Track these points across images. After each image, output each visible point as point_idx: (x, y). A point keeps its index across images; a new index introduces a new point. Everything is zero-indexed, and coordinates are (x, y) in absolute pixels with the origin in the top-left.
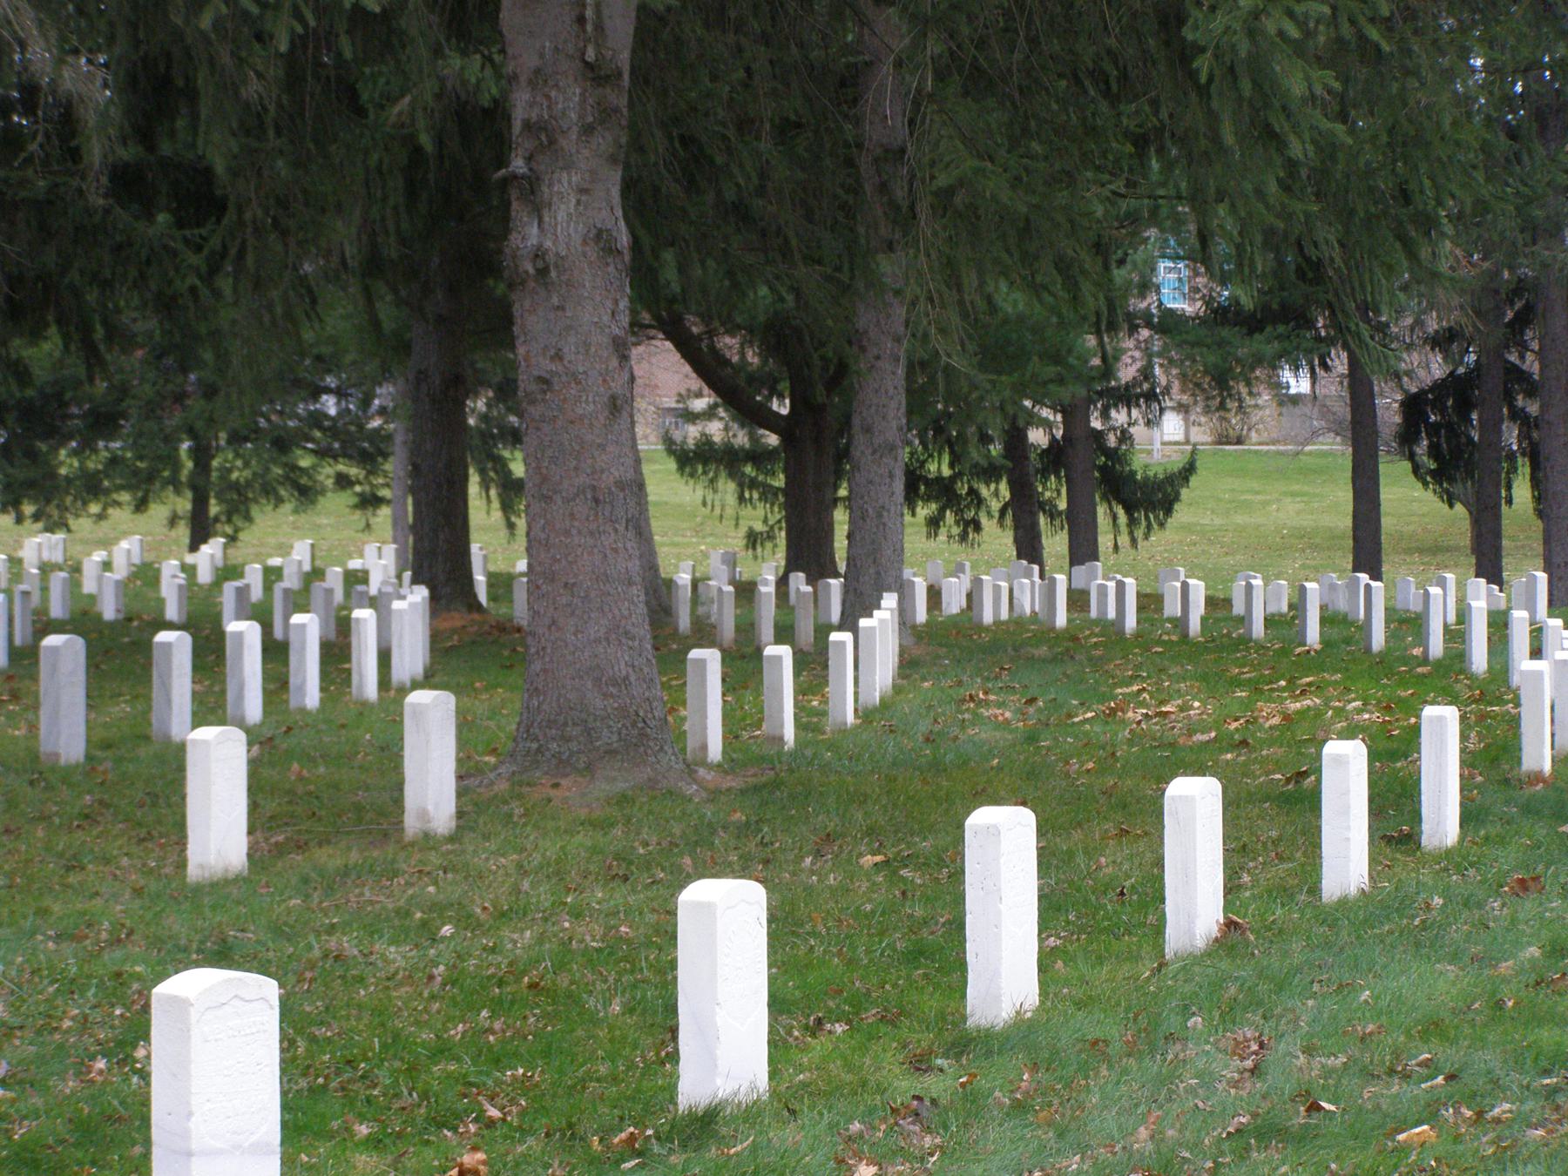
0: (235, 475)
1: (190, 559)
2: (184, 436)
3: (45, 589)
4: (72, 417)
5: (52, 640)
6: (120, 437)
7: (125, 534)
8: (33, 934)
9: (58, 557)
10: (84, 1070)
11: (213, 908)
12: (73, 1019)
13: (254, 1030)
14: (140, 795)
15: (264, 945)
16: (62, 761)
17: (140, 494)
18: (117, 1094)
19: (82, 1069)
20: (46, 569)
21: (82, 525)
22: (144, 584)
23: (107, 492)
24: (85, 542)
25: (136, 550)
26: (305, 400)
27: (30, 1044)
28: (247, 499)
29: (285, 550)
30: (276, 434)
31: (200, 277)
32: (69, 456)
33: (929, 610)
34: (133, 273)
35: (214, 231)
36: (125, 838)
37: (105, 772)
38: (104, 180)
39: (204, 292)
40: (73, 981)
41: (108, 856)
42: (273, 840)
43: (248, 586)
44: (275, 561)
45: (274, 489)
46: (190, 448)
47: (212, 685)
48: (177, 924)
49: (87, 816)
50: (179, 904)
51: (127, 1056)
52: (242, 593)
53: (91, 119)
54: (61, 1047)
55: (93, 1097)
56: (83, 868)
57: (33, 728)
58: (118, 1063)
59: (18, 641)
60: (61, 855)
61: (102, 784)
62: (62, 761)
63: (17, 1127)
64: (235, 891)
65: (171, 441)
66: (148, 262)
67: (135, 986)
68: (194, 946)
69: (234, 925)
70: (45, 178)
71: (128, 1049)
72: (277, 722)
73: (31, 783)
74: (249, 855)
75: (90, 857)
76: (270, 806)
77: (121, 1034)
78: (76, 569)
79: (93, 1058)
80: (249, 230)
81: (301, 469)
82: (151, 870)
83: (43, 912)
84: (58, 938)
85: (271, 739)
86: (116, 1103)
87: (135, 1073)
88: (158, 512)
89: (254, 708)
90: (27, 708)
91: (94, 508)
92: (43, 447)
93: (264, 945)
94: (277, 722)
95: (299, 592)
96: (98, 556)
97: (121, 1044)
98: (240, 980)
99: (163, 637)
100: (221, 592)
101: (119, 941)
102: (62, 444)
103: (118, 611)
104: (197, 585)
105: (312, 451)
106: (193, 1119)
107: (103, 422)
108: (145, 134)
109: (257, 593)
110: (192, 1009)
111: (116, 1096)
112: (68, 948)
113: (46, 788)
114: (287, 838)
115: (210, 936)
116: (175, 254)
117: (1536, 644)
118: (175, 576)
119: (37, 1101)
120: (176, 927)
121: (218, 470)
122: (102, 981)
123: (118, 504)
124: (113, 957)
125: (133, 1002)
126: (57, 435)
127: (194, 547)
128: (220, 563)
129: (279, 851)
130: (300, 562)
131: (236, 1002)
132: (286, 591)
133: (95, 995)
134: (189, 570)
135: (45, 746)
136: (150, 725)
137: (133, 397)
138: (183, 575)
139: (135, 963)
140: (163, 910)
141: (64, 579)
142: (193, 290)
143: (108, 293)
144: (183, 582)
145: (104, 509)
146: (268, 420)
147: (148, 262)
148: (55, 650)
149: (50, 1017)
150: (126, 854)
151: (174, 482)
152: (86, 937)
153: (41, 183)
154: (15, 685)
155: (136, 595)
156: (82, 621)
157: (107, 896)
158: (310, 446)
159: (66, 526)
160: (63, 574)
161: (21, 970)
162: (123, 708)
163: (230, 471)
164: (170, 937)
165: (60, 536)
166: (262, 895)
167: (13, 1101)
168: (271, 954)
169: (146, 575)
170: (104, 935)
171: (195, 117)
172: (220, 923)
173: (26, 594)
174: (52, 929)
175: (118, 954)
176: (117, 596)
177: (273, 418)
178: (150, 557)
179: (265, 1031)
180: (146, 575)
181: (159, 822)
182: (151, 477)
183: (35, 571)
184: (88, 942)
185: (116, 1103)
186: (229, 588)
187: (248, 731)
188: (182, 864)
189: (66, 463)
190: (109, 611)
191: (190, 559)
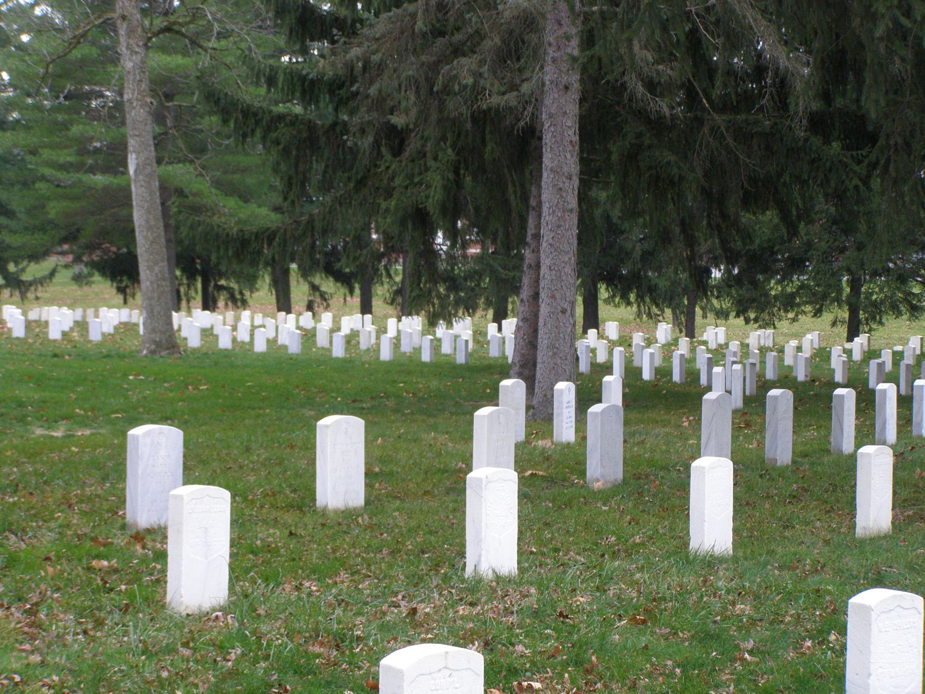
0: (874, 297)
1: (848, 346)
2: (845, 273)
3: (763, 362)
4: (778, 260)
5: (774, 392)
6: (806, 273)
7: (809, 331)
8: (765, 566)
9: (770, 343)
10: (798, 646)
11: (872, 553)
12: (791, 616)
13: (909, 626)
14: (827, 485)
15: (903, 576)
16: (779, 464)
17: (818, 306)
18: (819, 662)
19: (798, 646)
20: (763, 350)
21: (784, 325)
22: (821, 360)
23: (799, 305)
24: (786, 335)
25: (816, 341)
26: (917, 252)
27: (766, 630)
28: (881, 311)
29: (905, 342)
30: (899, 272)
31: (861, 180)
32: (776, 283)
33: (548, 400)
34: (821, 176)
35: (870, 152)
36: (818, 510)
37: (804, 471)
38: (805, 122)
39: (862, 188)
40: (790, 593)
41: (807, 520)
42: (906, 514)
43: (884, 362)
44: (899, 348)
45: (898, 306)
46: (848, 279)
47: (865, 420)
48: (851, 562)
49: (794, 497)
50: (852, 550)
51: (824, 639)
52: (881, 366)
53: (799, 86)
54: (785, 632)
55: (804, 662)
56: (793, 527)
57: (761, 444)
58: (818, 643)
59: (747, 393)
60: (780, 519)
61: (802, 478)
62: (779, 464)
63: (760, 679)
64: (885, 544)
65: (837, 275)
66: (830, 170)
67: (828, 598)
68: (862, 576)
69: (885, 564)
70: (770, 120)
71: (825, 635)
72: (906, 444)
73: (761, 476)
74: (893, 523)
75: (797, 521)
76: (905, 494)
77: (821, 626)
78: (781, 351)
79: (804, 639)
80: (892, 150)
81: (913, 294)
82: (834, 530)
83: (772, 553)
84: (780, 568)
85: (902, 454)
86: (819, 666)
87: (829, 650)
88: (827, 317)
89: (891, 434)
90: (755, 432)
91: (791, 315)
92: (760, 277)
93: (903, 576)
94: (906, 444)
95: (913, 366)
96: (794, 343)
97: (820, 632)
98: (901, 596)
99: (839, 391)
100: (868, 365)
101: (817, 570)
102: (772, 277)
103: (806, 376)
104: (852, 361)
105: (921, 282)
106: (871, 677)
107: (796, 264)
108: (826, 97)
109: (889, 367)
110: (873, 613)
111: (819, 663)
112: (787, 574)
113: (769, 479)
114: (914, 513)
115: (871, 570)
116: (846, 165)
117: (581, 434)
118: (840, 356)
119: (771, 664)
120: (850, 564)
121: (865, 293)
122: (807, 593)
123: (804, 313)
124: (813, 581)
125: (827, 607)
126: (769, 272)
127: (850, 339)
128: (866, 349)
129: (910, 520)
130: (914, 349)
131: (899, 609)
132: (908, 366)
133: (804, 602)
134: (849, 352)
135: (769, 454)
136: (830, 443)
137: (814, 249)
138: (845, 355)
139: (827, 584)
140: (842, 553)
141: (775, 356)
142: (856, 187)
143: (805, 188)
144: (846, 359)
145: (797, 315)
146: (895, 264)
147: (830, 170)
148: (775, 398)
149: (778, 614)
150: (819, 520)
151: (838, 300)
152: (797, 568)
153: (767, 123)
154: (748, 417)
155: (816, 367)
156: (786, 380)
157: (808, 544)
158: (919, 279)
159: (774, 325)
160: (774, 353)
161: (759, 585)
162: (812, 433)
163: (872, 294)
164: (847, 570)
165: (770, 331)
166: (901, 546)
167: (757, 664)
168: (908, 581)
169: (822, 355)
170: (808, 567)
171: (860, 83)
172: (877, 562)
173: (753, 365)
174: (777, 563)
175: (817, 578)
176: (806, 367)
177: (898, 262)
178: (823, 345)
179: (915, 627)
180: (822, 355)
181: (838, 502)
182: (825, 297)
183: (757, 351)
184: (798, 571)
185: (819, 666)
186: (873, 363)
187: (891, 447)
188: (853, 526)
189: (774, 288)
190: (801, 377)
191: (848, 346)
